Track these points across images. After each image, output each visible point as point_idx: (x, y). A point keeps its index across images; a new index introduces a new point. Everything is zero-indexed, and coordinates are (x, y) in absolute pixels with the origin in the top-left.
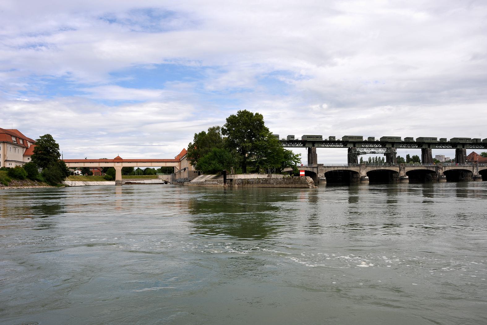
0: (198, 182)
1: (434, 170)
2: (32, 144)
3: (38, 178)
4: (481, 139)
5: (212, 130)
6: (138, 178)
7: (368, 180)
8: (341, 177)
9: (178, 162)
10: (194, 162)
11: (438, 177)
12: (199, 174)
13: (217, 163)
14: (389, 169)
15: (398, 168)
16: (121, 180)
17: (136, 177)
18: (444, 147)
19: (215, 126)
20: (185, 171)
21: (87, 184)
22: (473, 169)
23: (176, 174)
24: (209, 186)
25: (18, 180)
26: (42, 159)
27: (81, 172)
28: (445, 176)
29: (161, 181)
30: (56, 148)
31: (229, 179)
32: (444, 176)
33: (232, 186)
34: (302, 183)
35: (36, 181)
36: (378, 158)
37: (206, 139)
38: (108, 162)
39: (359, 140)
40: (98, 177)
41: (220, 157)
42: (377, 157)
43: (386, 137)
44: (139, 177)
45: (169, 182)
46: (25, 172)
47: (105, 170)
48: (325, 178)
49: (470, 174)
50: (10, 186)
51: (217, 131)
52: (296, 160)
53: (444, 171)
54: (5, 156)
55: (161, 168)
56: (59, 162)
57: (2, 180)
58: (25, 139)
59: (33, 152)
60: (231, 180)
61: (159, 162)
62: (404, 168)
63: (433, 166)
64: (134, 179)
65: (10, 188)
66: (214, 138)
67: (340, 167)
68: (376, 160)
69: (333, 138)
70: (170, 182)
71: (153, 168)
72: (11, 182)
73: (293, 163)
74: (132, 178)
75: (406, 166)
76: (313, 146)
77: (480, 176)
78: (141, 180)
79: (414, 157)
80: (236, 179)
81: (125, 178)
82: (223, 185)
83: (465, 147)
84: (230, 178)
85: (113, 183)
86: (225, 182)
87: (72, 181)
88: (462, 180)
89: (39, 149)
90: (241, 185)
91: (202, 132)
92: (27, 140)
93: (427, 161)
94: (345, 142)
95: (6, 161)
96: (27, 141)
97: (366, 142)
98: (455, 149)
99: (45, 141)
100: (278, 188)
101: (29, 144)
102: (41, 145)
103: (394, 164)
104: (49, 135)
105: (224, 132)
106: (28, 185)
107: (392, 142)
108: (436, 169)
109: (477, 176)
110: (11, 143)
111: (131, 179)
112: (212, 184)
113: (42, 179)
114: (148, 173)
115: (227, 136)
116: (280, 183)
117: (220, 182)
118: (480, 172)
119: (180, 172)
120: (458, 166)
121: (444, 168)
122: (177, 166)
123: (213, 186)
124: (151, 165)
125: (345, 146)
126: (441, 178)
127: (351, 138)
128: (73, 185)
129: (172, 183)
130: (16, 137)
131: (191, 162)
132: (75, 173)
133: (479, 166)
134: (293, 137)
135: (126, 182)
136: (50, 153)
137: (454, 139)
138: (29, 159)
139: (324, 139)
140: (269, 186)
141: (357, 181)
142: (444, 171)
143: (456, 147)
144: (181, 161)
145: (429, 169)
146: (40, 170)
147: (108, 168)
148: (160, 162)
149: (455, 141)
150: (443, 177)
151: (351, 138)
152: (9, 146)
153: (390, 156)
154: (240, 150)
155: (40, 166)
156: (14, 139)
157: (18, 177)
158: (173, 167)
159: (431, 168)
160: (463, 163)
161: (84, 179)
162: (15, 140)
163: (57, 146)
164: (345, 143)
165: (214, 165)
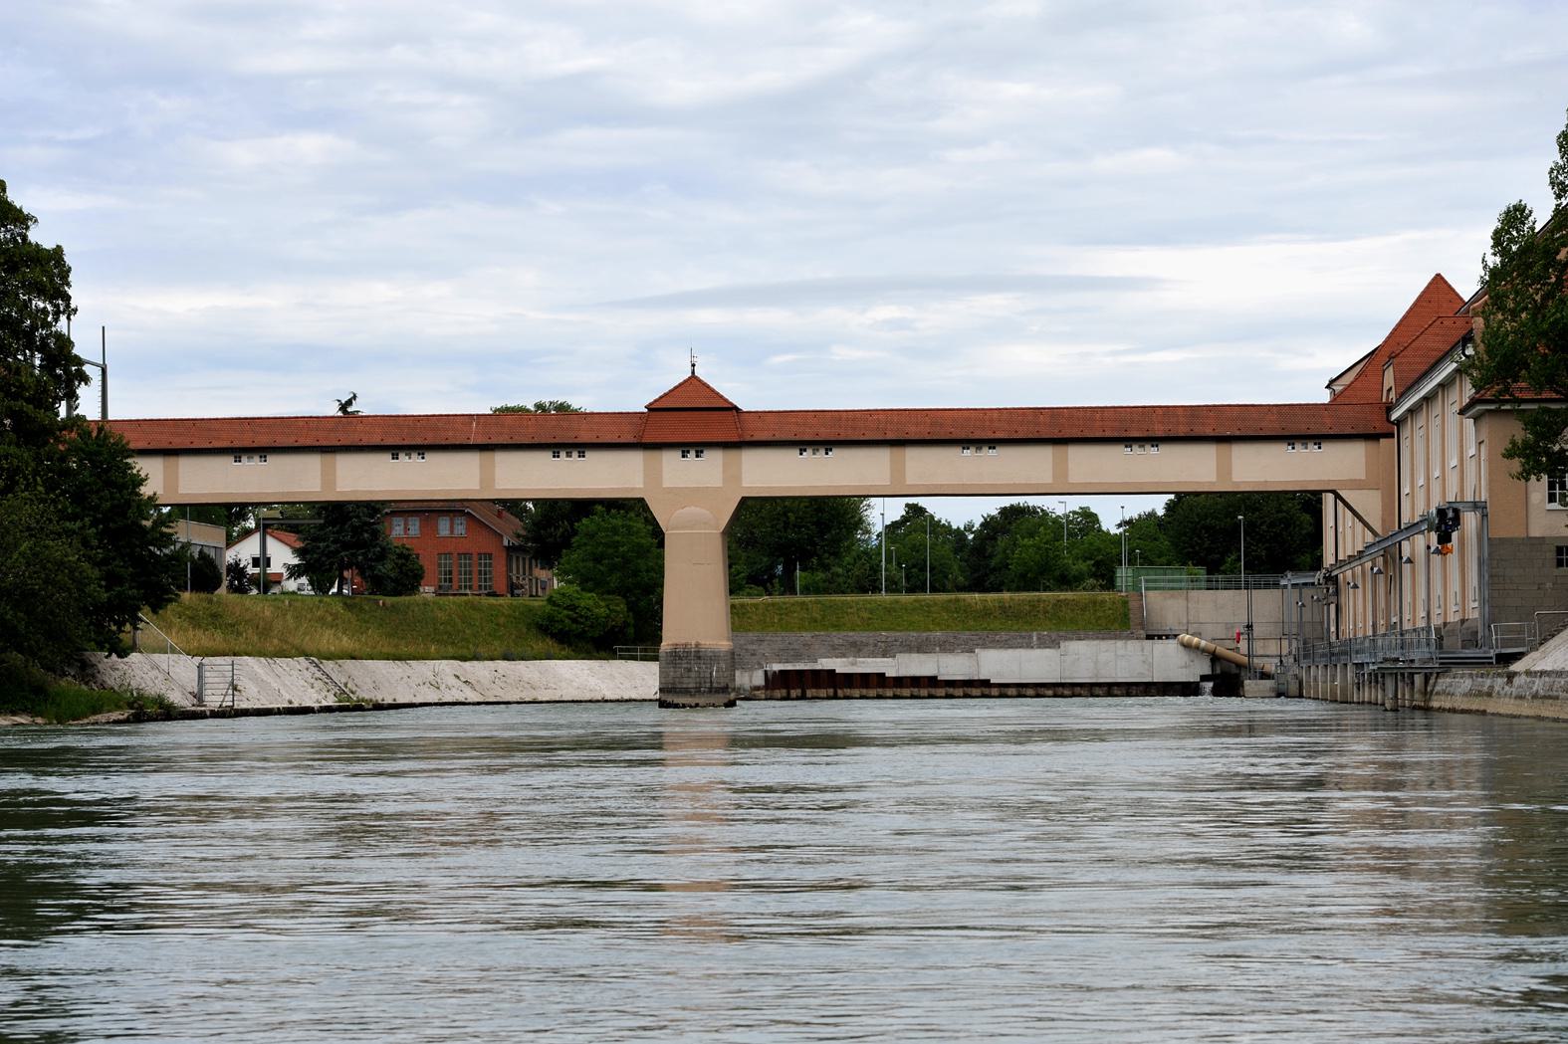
6: (912, 626)
17: (889, 610)
20: (1445, 538)
21: (366, 693)
23: (1346, 575)
27: (299, 552)
29: (1168, 661)
30: (41, 292)
40: (474, 607)
44: (926, 609)
45: (1265, 676)
55: (1170, 507)
56: (74, 450)
70: (1271, 666)
71: (1074, 503)
74: (837, 627)
78: (946, 647)
85: (639, 678)
111: (837, 637)
119: (1387, 555)
122: (1357, 485)
124: (1061, 470)
128: (213, 701)
129: (1293, 688)
131: (1517, 431)
132: (236, 570)
135: (777, 667)
144: (1406, 433)
147: (582, 507)
158: (1310, 502)
161: (327, 639)
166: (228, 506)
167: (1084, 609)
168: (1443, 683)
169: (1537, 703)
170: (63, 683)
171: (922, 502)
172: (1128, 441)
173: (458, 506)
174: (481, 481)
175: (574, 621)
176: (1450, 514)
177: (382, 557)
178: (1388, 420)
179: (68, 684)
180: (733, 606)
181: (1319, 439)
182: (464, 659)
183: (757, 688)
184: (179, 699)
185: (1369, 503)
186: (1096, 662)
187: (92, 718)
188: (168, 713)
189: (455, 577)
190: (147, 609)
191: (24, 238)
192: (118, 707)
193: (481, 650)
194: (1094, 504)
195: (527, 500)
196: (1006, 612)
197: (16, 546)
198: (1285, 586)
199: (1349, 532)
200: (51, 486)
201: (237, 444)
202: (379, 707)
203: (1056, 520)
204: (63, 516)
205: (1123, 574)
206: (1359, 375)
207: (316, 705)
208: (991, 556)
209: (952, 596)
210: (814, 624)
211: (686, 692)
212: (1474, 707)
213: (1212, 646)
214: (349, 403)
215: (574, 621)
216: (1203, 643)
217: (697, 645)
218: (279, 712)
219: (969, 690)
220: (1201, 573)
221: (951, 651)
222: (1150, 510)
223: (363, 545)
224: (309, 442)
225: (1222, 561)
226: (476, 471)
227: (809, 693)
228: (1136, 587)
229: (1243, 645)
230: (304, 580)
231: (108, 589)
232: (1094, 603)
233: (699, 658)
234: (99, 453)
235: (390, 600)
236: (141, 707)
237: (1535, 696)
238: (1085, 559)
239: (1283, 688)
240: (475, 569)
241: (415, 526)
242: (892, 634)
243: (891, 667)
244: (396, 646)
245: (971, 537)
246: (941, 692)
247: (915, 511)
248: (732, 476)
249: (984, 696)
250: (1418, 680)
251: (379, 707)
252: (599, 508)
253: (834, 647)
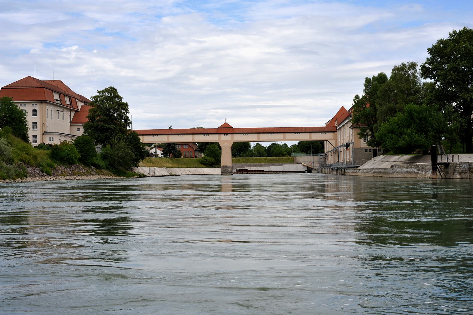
0: (376, 169)
2: (83, 104)
3: (96, 162)
5: (399, 71)
6: (259, 162)
9: (334, 132)
10: (365, 131)
12: (375, 155)
13: (416, 133)
16: (231, 165)
17: (256, 160)
19: (407, 61)
20: (347, 148)
21: (174, 173)
23: (329, 154)
24: (399, 176)
25: (66, 165)
26: (103, 130)
27: (162, 151)
29: (300, 168)
30: (124, 109)
31: (442, 164)
33: (448, 177)
35: (92, 166)
38: (208, 134)
40: (190, 159)
41: (420, 120)
44: (262, 160)
45: (316, 170)
46: (76, 150)
47: (203, 147)
50: (54, 175)
51: (410, 72)
54: (43, 124)
55: (299, 143)
56: (130, 134)
57: (43, 165)
58: (74, 97)
59: (88, 117)
60: (447, 165)
65: (54, 178)
66: (403, 85)
70: (316, 168)
71: (283, 143)
72: (55, 169)
74: (248, 162)
78: (265, 166)
80: (456, 164)
81: (238, 161)
84: (444, 161)
85: (218, 171)
86: (434, 168)
87: (150, 167)
89: (96, 114)
91: (379, 75)
92: (76, 98)
95: (45, 133)
96: (77, 100)
99: (106, 98)
100: (350, 176)
101: (80, 105)
102: (99, 106)
104: (113, 88)
105: (426, 73)
106: (81, 175)
110: (52, 104)
111: (248, 164)
112: (405, 173)
113: (102, 163)
115: (433, 80)
117: (422, 168)
119: (336, 151)
122: (331, 140)
123: (409, 176)
124: (284, 137)
128: (151, 174)
129: (320, 172)
130: (60, 94)
131: (359, 131)
132: (152, 154)
135: (238, 169)
136: (114, 120)
138: (79, 130)
144: (339, 131)
146: (98, 148)
147: (207, 143)
152: (49, 109)
154: (458, 106)
155: (99, 141)
156: (56, 96)
157: (66, 159)
158: (322, 143)
161: (167, 165)
162: (59, 99)
163: (125, 106)
165: (409, 135)
166: (149, 144)
167: (287, 159)
168: (347, 171)
169: (365, 174)
170: (128, 172)
172: (295, 133)
173: (187, 144)
175: (206, 162)
176: (348, 144)
177: (176, 151)
178: (336, 129)
179: (129, 172)
180: (232, 159)
181: (325, 132)
182: (189, 168)
183: (235, 172)
184: (146, 174)
185: (333, 142)
186: (289, 168)
187: (133, 177)
188: (145, 176)
189: (186, 155)
190: (141, 160)
191: (121, 101)
192: (137, 175)
193: (192, 166)
194: (287, 143)
195: (196, 142)
196: (274, 160)
197: (121, 150)
198: (319, 156)
199: (329, 147)
200: (126, 140)
201: (153, 134)
202: (176, 175)
203: (281, 146)
204: (129, 145)
205: (293, 154)
206: (330, 122)
207: (167, 175)
208: (270, 151)
209: (266, 157)
210: (244, 162)
211: (225, 173)
212: (353, 174)
213: (307, 165)
214: (171, 127)
215: (206, 162)
216: (306, 165)
217: (227, 165)
218: (161, 176)
219: (269, 172)
221: (266, 166)
222: (295, 144)
223: (174, 150)
224: (162, 133)
225: (308, 152)
226: (230, 138)
227: (243, 173)
228: (295, 156)
229: (312, 165)
230: (163, 155)
231: (135, 157)
232: (288, 158)
233: (227, 167)
234: (134, 135)
235: (177, 158)
236: (141, 175)
237: (364, 173)
238: (286, 152)
239: (318, 172)
240: (190, 153)
241: (180, 147)
242: (256, 164)
244: (178, 166)
245: (267, 148)
246: (264, 173)
247: (258, 144)
248: (232, 138)
249: (271, 173)
250: (343, 170)
251: (176, 175)
252: (210, 144)
253: (247, 166)
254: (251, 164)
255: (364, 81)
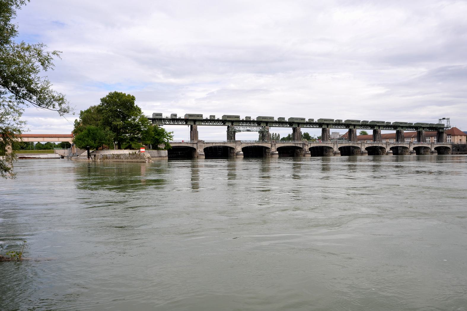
1: (301, 146)
4: (391, 122)
6: (33, 153)
7: (242, 155)
8: (220, 152)
9: (72, 137)
11: (304, 152)
14: (262, 145)
15: (270, 145)
17: (31, 152)
18: (339, 127)
22: (334, 146)
28: (310, 152)
29: (57, 156)
32: (308, 152)
34: (141, 158)
36: (274, 134)
37: (87, 117)
39: (236, 119)
42: (273, 134)
43: (323, 119)
48: (203, 153)
49: (331, 150)
52: (168, 137)
53: (309, 147)
61: (51, 137)
62: (275, 145)
63: (301, 143)
64: (29, 154)
67: (218, 143)
68: (273, 136)
69: (249, 118)
73: (165, 140)
74: (26, 153)
75: (276, 143)
76: (195, 124)
77: (391, 151)
78: (37, 155)
79: (305, 134)
82: (87, 160)
83: (329, 127)
88: (326, 155)
90: (102, 160)
93: (296, 139)
94: (224, 121)
97: (243, 121)
98: (322, 129)
103: (266, 141)
107: (232, 121)
108: (303, 146)
109: (336, 152)
111: (26, 154)
114: (48, 147)
116: (127, 158)
118: (367, 149)
120: (321, 144)
121: (309, 145)
124: (44, 140)
125: (224, 124)
126: (306, 153)
127: (229, 117)
133: (339, 144)
134: (176, 115)
135: (20, 157)
137: (321, 119)
139: (241, 119)
140: (120, 161)
141: (234, 156)
142: (310, 147)
143: (349, 127)
145: (297, 146)
148: (52, 137)
149: (348, 123)
150: (308, 152)
151: (229, 117)
153: (263, 135)
159: (298, 144)
160: (327, 140)
164: (259, 123)
165: (87, 141)
171: (55, 142)
174: (237, 141)
210: (24, 153)
220: (62, 148)
243: (31, 156)
254: (28, 154)
255: (80, 113)
